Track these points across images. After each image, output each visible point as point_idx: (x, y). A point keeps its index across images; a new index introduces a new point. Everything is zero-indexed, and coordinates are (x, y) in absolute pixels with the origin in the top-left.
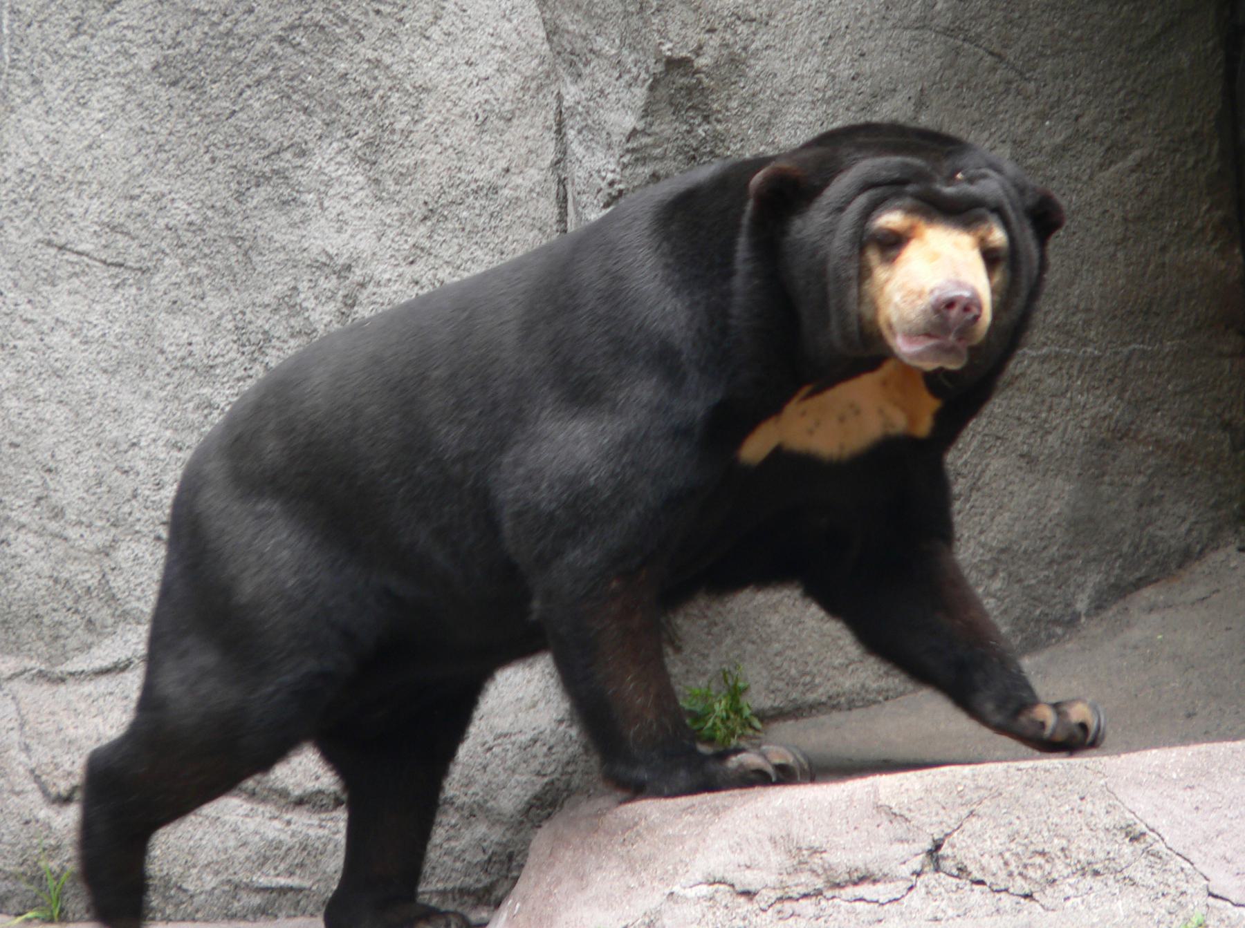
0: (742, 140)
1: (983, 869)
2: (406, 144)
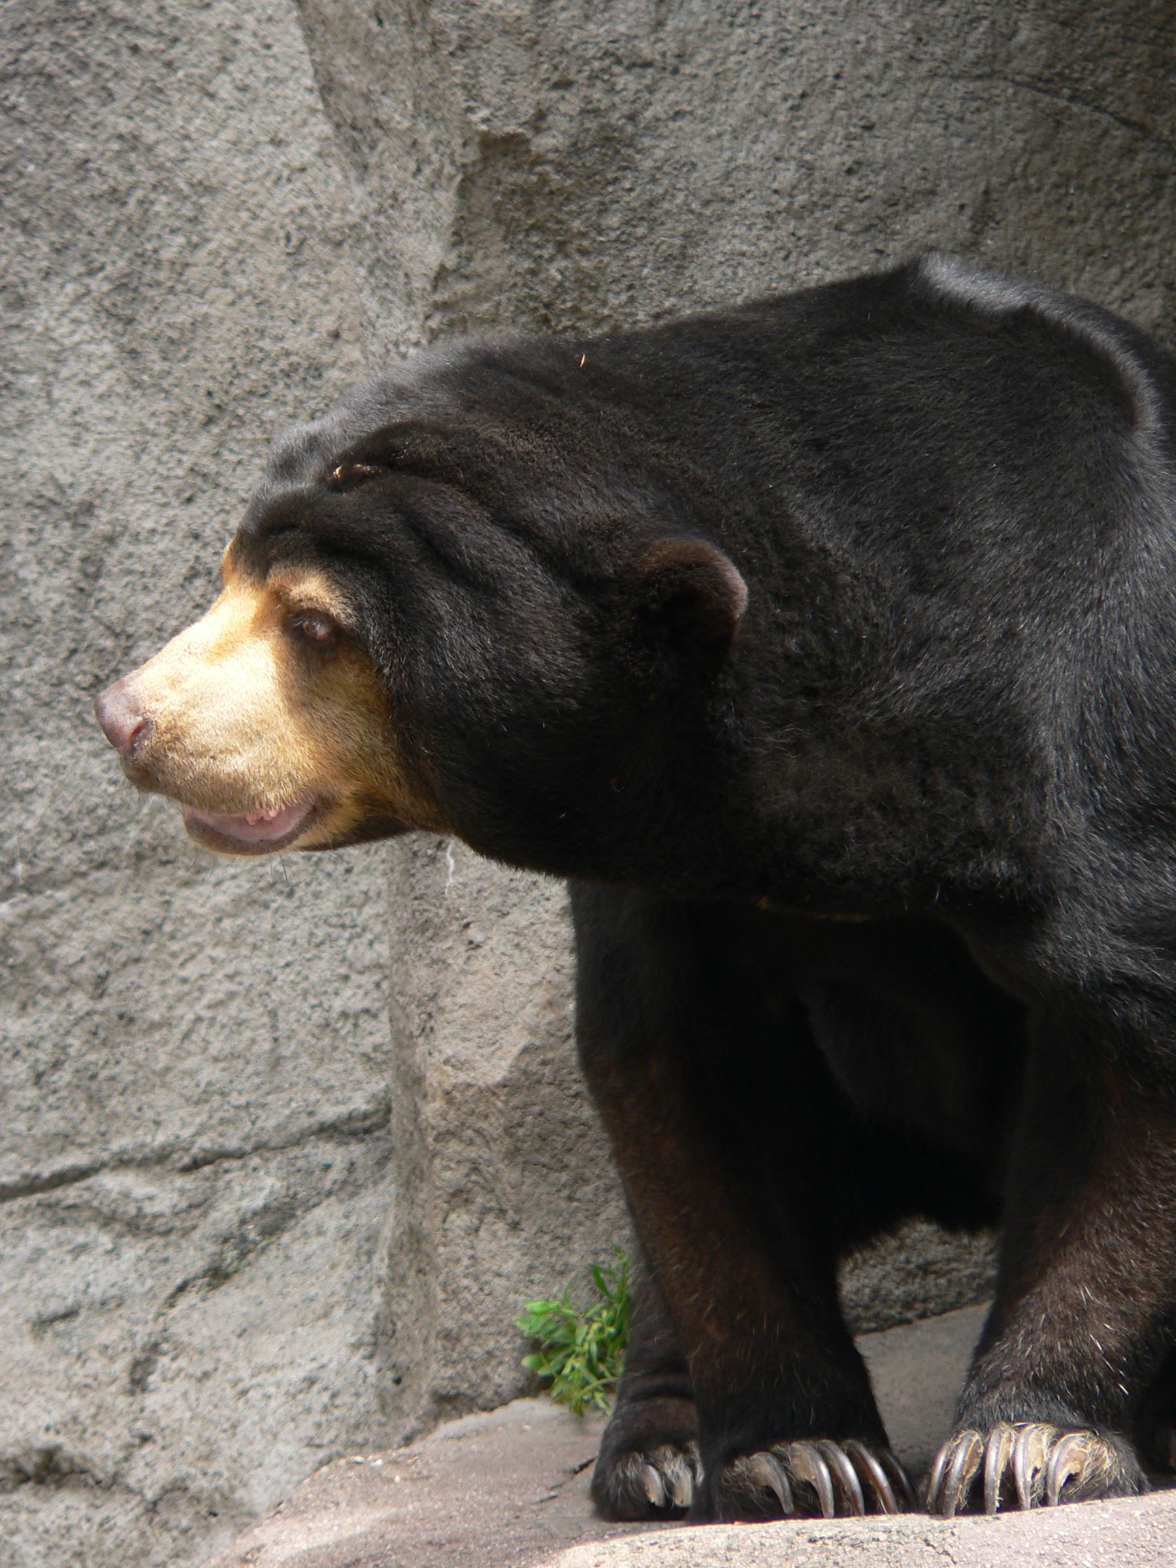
0: (630, 287)
2: (180, 287)
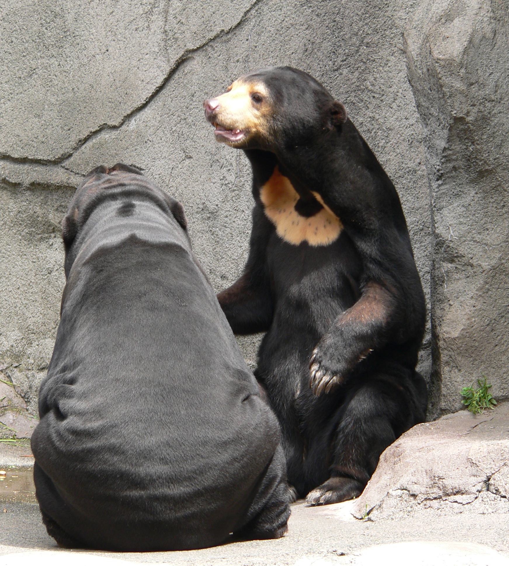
0: (488, 153)
1: (506, 491)
